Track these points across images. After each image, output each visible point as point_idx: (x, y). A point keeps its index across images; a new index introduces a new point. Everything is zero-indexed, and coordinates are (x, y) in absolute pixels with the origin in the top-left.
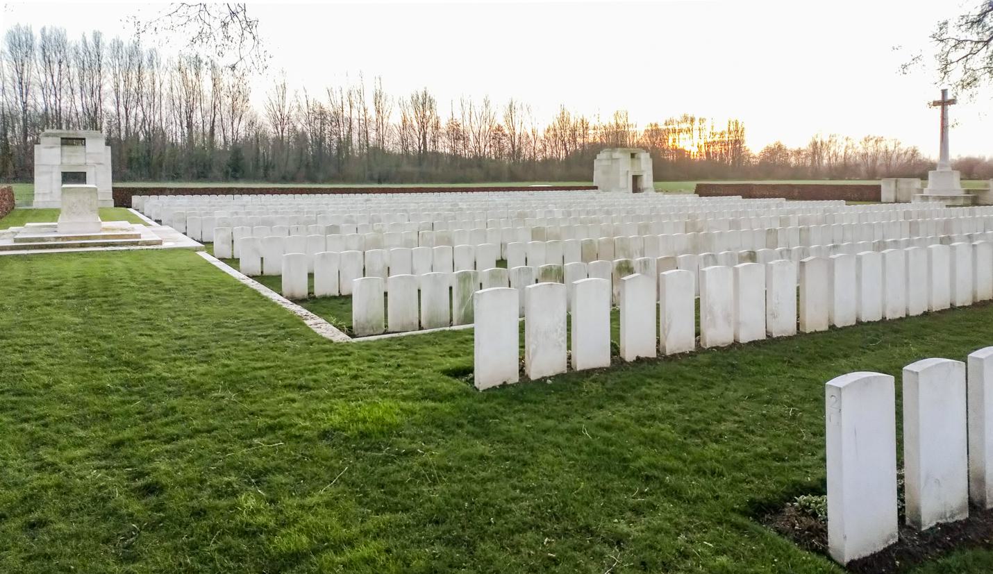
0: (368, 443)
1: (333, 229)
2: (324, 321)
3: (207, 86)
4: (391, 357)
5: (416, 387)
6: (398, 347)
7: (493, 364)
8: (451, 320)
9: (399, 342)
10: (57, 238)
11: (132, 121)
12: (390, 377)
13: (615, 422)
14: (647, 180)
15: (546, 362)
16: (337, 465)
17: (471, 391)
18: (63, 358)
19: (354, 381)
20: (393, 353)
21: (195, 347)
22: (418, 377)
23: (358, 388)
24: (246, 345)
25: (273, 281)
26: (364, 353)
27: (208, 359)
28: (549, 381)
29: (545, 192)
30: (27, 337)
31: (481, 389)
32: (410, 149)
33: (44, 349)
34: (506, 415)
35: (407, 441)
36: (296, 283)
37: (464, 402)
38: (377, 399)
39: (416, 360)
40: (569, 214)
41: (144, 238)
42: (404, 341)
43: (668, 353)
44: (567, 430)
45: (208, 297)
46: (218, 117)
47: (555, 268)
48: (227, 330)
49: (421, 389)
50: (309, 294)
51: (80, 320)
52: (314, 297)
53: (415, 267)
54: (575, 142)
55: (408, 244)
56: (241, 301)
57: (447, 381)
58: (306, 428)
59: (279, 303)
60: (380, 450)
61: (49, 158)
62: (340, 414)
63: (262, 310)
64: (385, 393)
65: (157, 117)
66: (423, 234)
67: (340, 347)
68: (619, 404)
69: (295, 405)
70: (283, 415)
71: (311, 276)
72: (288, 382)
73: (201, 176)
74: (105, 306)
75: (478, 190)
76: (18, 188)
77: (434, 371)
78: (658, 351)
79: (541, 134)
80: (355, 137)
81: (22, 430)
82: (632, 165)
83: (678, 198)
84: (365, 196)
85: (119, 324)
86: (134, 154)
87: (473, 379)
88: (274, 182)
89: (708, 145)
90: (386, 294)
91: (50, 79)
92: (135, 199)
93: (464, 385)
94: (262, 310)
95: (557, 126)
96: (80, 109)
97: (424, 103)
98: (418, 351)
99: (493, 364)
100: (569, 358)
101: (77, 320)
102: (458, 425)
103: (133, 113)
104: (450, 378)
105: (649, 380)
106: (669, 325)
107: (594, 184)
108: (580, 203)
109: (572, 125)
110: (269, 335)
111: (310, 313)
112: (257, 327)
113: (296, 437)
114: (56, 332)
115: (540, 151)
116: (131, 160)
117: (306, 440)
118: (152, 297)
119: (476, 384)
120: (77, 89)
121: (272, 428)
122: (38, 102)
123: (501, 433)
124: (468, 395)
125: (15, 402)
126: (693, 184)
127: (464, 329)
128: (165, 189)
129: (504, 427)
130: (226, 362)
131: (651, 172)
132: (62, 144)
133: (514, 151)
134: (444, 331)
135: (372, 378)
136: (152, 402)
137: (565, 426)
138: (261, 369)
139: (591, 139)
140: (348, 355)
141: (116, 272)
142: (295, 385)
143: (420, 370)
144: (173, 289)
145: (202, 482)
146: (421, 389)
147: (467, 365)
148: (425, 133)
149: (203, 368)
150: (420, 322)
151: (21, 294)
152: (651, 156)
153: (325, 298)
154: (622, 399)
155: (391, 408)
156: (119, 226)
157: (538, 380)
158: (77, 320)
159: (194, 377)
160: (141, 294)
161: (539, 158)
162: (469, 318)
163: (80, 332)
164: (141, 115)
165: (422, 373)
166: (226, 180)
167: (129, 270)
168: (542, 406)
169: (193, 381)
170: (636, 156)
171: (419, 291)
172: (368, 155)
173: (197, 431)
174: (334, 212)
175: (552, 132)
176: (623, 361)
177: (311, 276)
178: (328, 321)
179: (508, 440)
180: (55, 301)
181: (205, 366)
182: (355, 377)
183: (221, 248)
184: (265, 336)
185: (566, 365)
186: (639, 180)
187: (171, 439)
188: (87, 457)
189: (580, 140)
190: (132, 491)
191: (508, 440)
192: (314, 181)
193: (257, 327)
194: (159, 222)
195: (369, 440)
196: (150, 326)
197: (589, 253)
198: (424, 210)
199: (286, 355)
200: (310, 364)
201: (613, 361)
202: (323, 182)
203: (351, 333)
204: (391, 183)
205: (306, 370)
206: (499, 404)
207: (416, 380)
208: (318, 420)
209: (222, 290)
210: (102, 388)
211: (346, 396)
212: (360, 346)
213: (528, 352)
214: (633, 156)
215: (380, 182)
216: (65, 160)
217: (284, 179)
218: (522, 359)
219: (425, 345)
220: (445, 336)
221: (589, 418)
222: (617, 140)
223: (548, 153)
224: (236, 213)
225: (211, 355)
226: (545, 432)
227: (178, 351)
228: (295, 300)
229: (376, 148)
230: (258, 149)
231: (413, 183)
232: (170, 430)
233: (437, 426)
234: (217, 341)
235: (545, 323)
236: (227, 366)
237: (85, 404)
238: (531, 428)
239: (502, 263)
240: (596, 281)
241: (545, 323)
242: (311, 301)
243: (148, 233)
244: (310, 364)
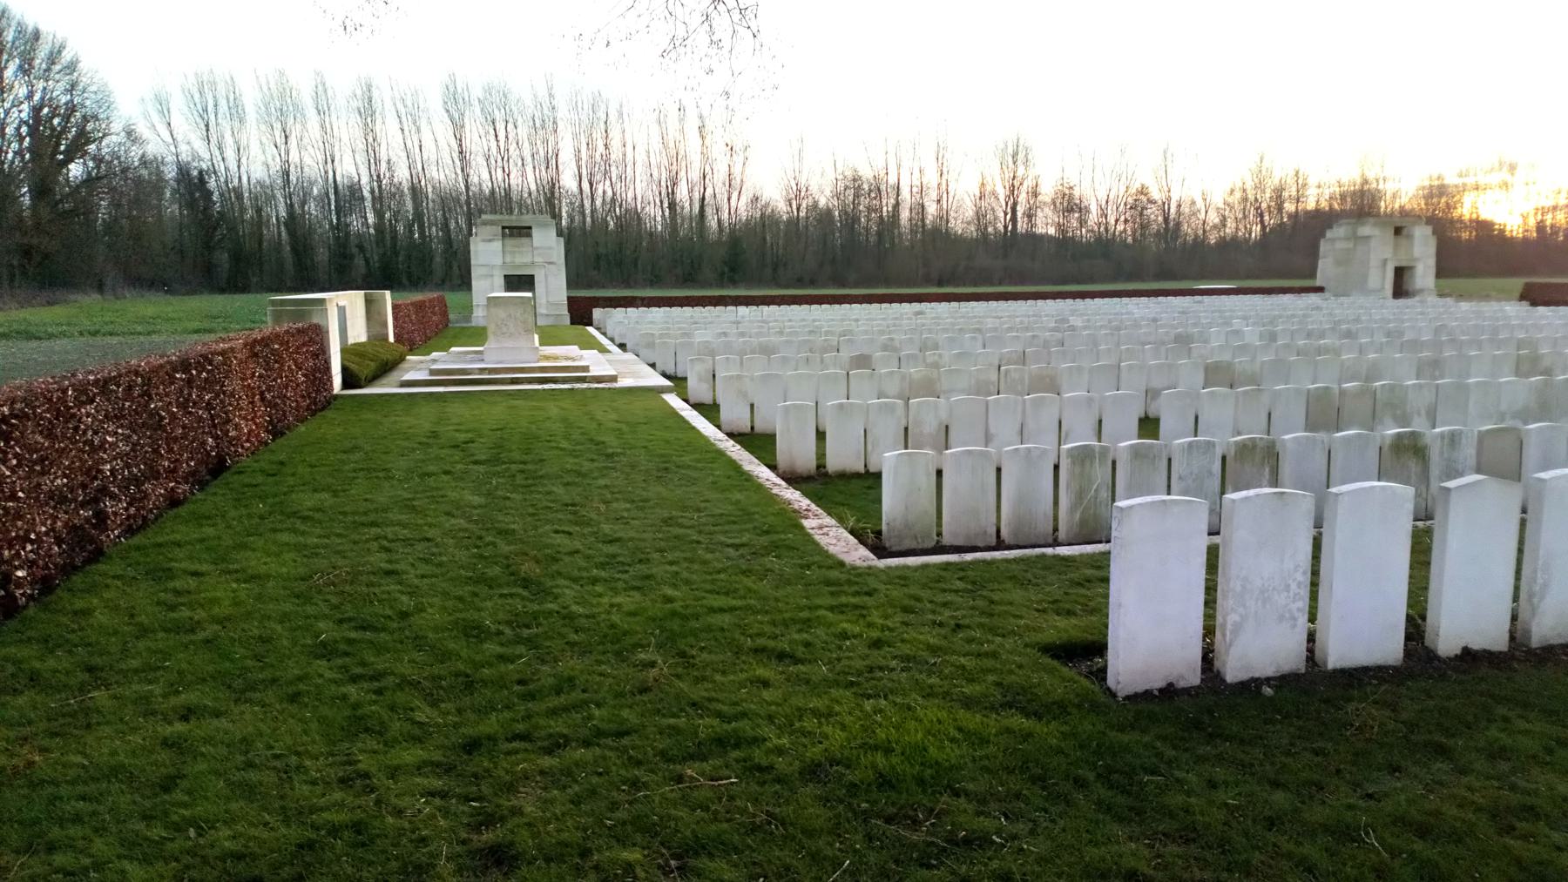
0: (893, 804)
1: (862, 361)
2: (833, 522)
3: (693, 146)
4: (945, 605)
5: (991, 678)
6: (959, 585)
7: (1149, 635)
8: (1056, 530)
9: (962, 574)
10: (482, 370)
11: (598, 202)
12: (940, 648)
13: (1437, 813)
14: (1424, 274)
15: (1261, 647)
16: (829, 853)
17: (1103, 699)
18: (440, 565)
19: (876, 652)
20: (949, 597)
21: (628, 560)
22: (994, 655)
23: (881, 669)
24: (705, 562)
25: (759, 442)
26: (896, 593)
27: (643, 584)
28: (1268, 691)
29: (1223, 297)
30: (405, 526)
31: (1121, 694)
32: (990, 229)
33: (420, 547)
34: (1179, 768)
35: (971, 808)
36: (797, 449)
37: (1088, 726)
38: (915, 699)
39: (992, 615)
40: (1273, 337)
41: (595, 371)
42: (970, 573)
43: (1535, 642)
44: (1326, 829)
45: (664, 471)
46: (709, 191)
47: (1260, 444)
48: (681, 531)
49: (999, 684)
50: (818, 467)
51: (482, 500)
52: (826, 474)
53: (992, 430)
54: (1280, 208)
55: (981, 389)
56: (710, 479)
57: (1051, 671)
58: (780, 751)
59: (768, 484)
60: (915, 824)
61: (489, 256)
62: (843, 727)
63: (738, 496)
64: (931, 687)
65: (630, 195)
66: (1007, 371)
67: (857, 575)
68: (1441, 766)
69: (767, 695)
70: (744, 715)
71: (821, 435)
72: (761, 642)
73: (689, 279)
74: (519, 480)
75: (1103, 295)
76: (452, 298)
77: (1026, 645)
78: (1512, 638)
79: (1218, 201)
80: (905, 215)
81: (344, 697)
82: (1396, 247)
83: (1490, 308)
84: (916, 306)
85: (531, 510)
86: (602, 250)
87: (1104, 670)
88: (787, 287)
89: (1544, 212)
90: (939, 473)
91: (493, 144)
92: (597, 313)
93: (1085, 682)
94: (738, 496)
95: (1249, 185)
96: (533, 187)
97: (1017, 155)
98: (996, 597)
99: (1149, 635)
100: (1311, 638)
101: (476, 500)
102: (1076, 781)
103: (600, 192)
104: (1055, 663)
105: (1501, 710)
106: (1545, 586)
107: (1318, 283)
108: (1293, 316)
109: (1276, 182)
110: (743, 545)
111: (813, 507)
112: (727, 528)
113: (760, 769)
114: (443, 519)
115: (1215, 227)
116: (598, 257)
117: (778, 780)
118: (587, 466)
119: (1111, 682)
120: (528, 159)
121: (722, 743)
122: (481, 177)
123: (1172, 816)
124: (1095, 707)
125: (350, 642)
126: (1518, 283)
127: (1081, 555)
128: (634, 298)
129: (1176, 800)
130: (670, 592)
131: (1432, 262)
132: (504, 235)
133: (1167, 229)
134: (1044, 555)
135: (906, 650)
136: (544, 662)
137: (1316, 814)
138: (722, 610)
139: (1311, 205)
140: (869, 594)
141: (548, 424)
142: (773, 650)
143: (998, 639)
144: (618, 454)
145: (585, 853)
146: (999, 684)
147: (1090, 638)
148: (1015, 204)
149: (627, 601)
150: (998, 531)
151: (419, 455)
152: (1434, 233)
153: (844, 476)
154: (1442, 751)
155: (939, 722)
156: (569, 354)
157: (1242, 683)
158: (476, 500)
159: (616, 618)
160: (572, 460)
161: (1213, 239)
162: (1095, 530)
163: (476, 522)
164: (610, 193)
165: (1001, 645)
166: (721, 286)
167: (564, 420)
168: (1258, 753)
169: (613, 626)
170: (1405, 232)
171: (999, 470)
172: (923, 241)
173: (600, 733)
174: (866, 332)
175: (1238, 195)
176: (1431, 656)
177: (821, 435)
178: (841, 521)
179: (1189, 834)
180: (459, 466)
181: (637, 595)
182: (877, 644)
183: (698, 387)
184: (736, 547)
185: (1305, 654)
186: (1405, 278)
187: (555, 745)
188: (419, 768)
189: (1289, 207)
190: (472, 854)
191: (1189, 834)
192: (627, 284)
193: (727, 528)
194: (622, 346)
195: (894, 795)
196: (570, 517)
197: (1324, 413)
198: (1010, 329)
199: (765, 587)
200: (801, 609)
201: (1408, 653)
202: (856, 286)
203: (880, 551)
204: (958, 285)
205: (794, 621)
206: (1164, 738)
207: (989, 663)
208: (805, 733)
209: (687, 459)
210: (477, 628)
211: (858, 684)
212: (903, 577)
213: (1224, 626)
214: (1398, 231)
215: (940, 284)
216: (508, 260)
217: (800, 282)
218: (1209, 631)
219: (1009, 585)
220: (1046, 568)
221: (1370, 796)
222: (1361, 206)
223: (1231, 225)
224: (725, 334)
225: (648, 577)
226: (1271, 823)
227: (602, 566)
228: (793, 479)
229: (936, 231)
230: (764, 239)
231: (992, 284)
232: (559, 726)
233: (1034, 780)
234: (661, 551)
235: (1266, 564)
236: (669, 600)
237: (445, 656)
238: (1237, 808)
239: (1149, 426)
240: (1383, 488)
241: (1266, 564)
242: (820, 483)
243: (597, 364)
244: (801, 609)
